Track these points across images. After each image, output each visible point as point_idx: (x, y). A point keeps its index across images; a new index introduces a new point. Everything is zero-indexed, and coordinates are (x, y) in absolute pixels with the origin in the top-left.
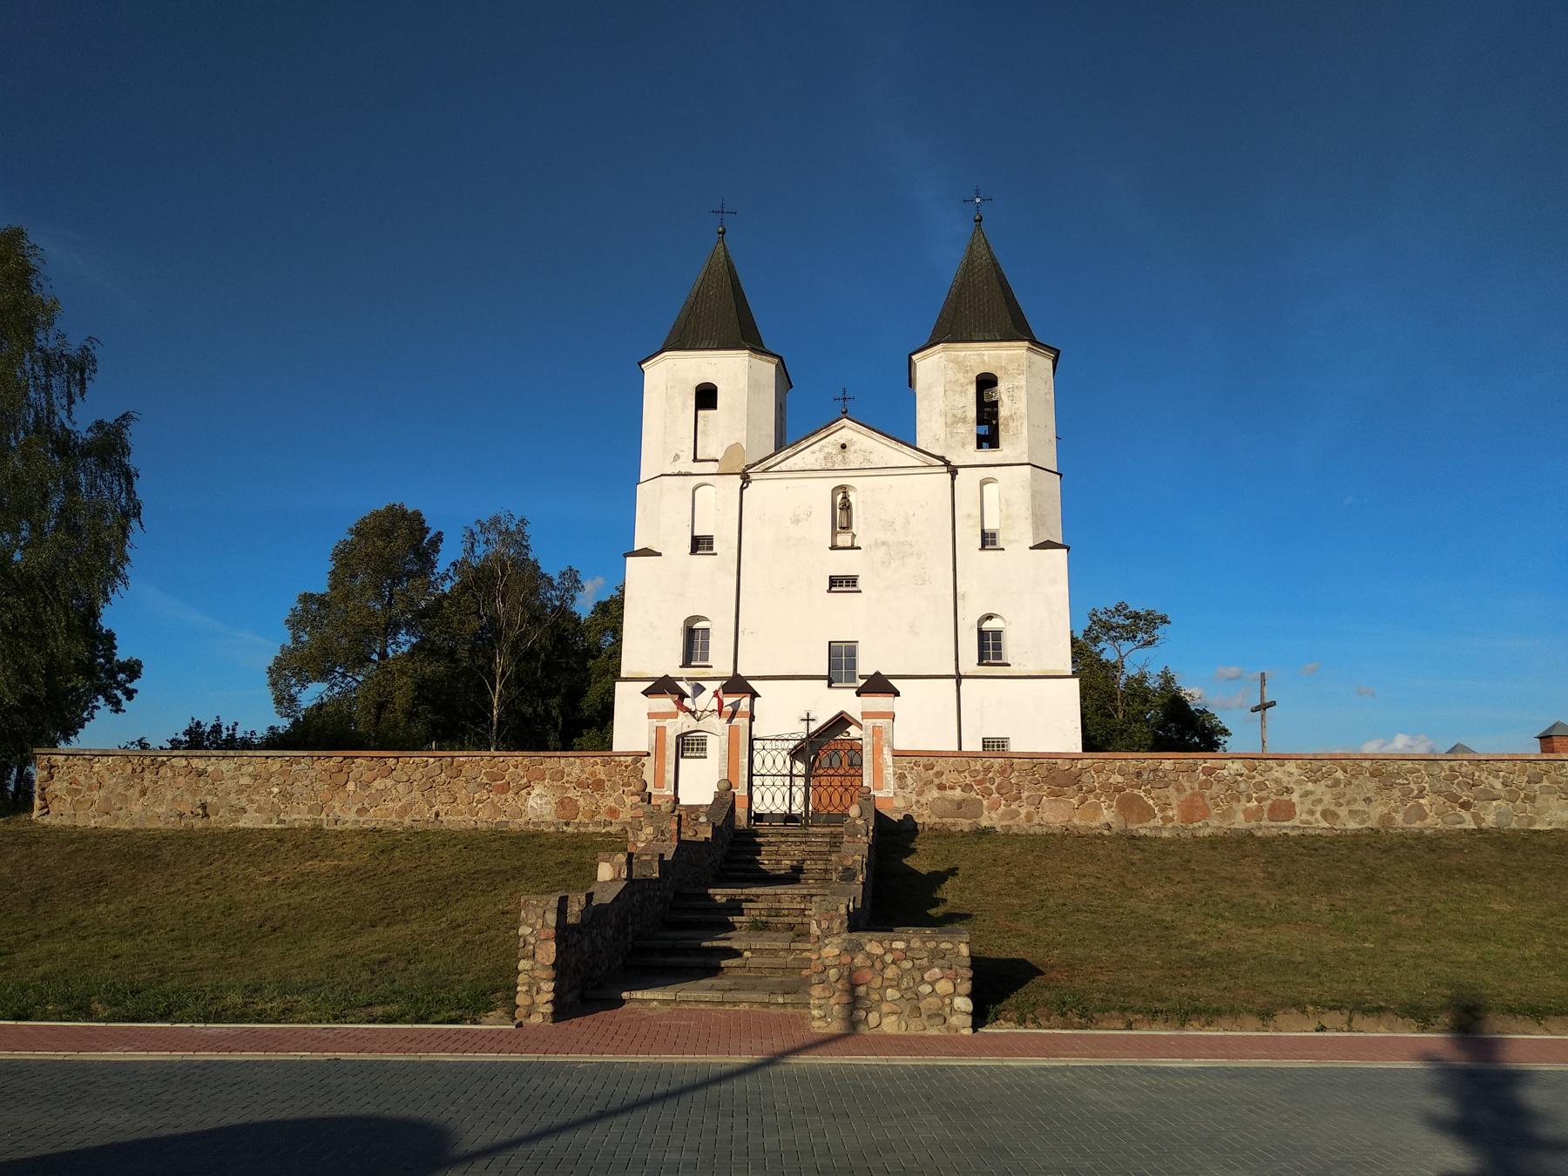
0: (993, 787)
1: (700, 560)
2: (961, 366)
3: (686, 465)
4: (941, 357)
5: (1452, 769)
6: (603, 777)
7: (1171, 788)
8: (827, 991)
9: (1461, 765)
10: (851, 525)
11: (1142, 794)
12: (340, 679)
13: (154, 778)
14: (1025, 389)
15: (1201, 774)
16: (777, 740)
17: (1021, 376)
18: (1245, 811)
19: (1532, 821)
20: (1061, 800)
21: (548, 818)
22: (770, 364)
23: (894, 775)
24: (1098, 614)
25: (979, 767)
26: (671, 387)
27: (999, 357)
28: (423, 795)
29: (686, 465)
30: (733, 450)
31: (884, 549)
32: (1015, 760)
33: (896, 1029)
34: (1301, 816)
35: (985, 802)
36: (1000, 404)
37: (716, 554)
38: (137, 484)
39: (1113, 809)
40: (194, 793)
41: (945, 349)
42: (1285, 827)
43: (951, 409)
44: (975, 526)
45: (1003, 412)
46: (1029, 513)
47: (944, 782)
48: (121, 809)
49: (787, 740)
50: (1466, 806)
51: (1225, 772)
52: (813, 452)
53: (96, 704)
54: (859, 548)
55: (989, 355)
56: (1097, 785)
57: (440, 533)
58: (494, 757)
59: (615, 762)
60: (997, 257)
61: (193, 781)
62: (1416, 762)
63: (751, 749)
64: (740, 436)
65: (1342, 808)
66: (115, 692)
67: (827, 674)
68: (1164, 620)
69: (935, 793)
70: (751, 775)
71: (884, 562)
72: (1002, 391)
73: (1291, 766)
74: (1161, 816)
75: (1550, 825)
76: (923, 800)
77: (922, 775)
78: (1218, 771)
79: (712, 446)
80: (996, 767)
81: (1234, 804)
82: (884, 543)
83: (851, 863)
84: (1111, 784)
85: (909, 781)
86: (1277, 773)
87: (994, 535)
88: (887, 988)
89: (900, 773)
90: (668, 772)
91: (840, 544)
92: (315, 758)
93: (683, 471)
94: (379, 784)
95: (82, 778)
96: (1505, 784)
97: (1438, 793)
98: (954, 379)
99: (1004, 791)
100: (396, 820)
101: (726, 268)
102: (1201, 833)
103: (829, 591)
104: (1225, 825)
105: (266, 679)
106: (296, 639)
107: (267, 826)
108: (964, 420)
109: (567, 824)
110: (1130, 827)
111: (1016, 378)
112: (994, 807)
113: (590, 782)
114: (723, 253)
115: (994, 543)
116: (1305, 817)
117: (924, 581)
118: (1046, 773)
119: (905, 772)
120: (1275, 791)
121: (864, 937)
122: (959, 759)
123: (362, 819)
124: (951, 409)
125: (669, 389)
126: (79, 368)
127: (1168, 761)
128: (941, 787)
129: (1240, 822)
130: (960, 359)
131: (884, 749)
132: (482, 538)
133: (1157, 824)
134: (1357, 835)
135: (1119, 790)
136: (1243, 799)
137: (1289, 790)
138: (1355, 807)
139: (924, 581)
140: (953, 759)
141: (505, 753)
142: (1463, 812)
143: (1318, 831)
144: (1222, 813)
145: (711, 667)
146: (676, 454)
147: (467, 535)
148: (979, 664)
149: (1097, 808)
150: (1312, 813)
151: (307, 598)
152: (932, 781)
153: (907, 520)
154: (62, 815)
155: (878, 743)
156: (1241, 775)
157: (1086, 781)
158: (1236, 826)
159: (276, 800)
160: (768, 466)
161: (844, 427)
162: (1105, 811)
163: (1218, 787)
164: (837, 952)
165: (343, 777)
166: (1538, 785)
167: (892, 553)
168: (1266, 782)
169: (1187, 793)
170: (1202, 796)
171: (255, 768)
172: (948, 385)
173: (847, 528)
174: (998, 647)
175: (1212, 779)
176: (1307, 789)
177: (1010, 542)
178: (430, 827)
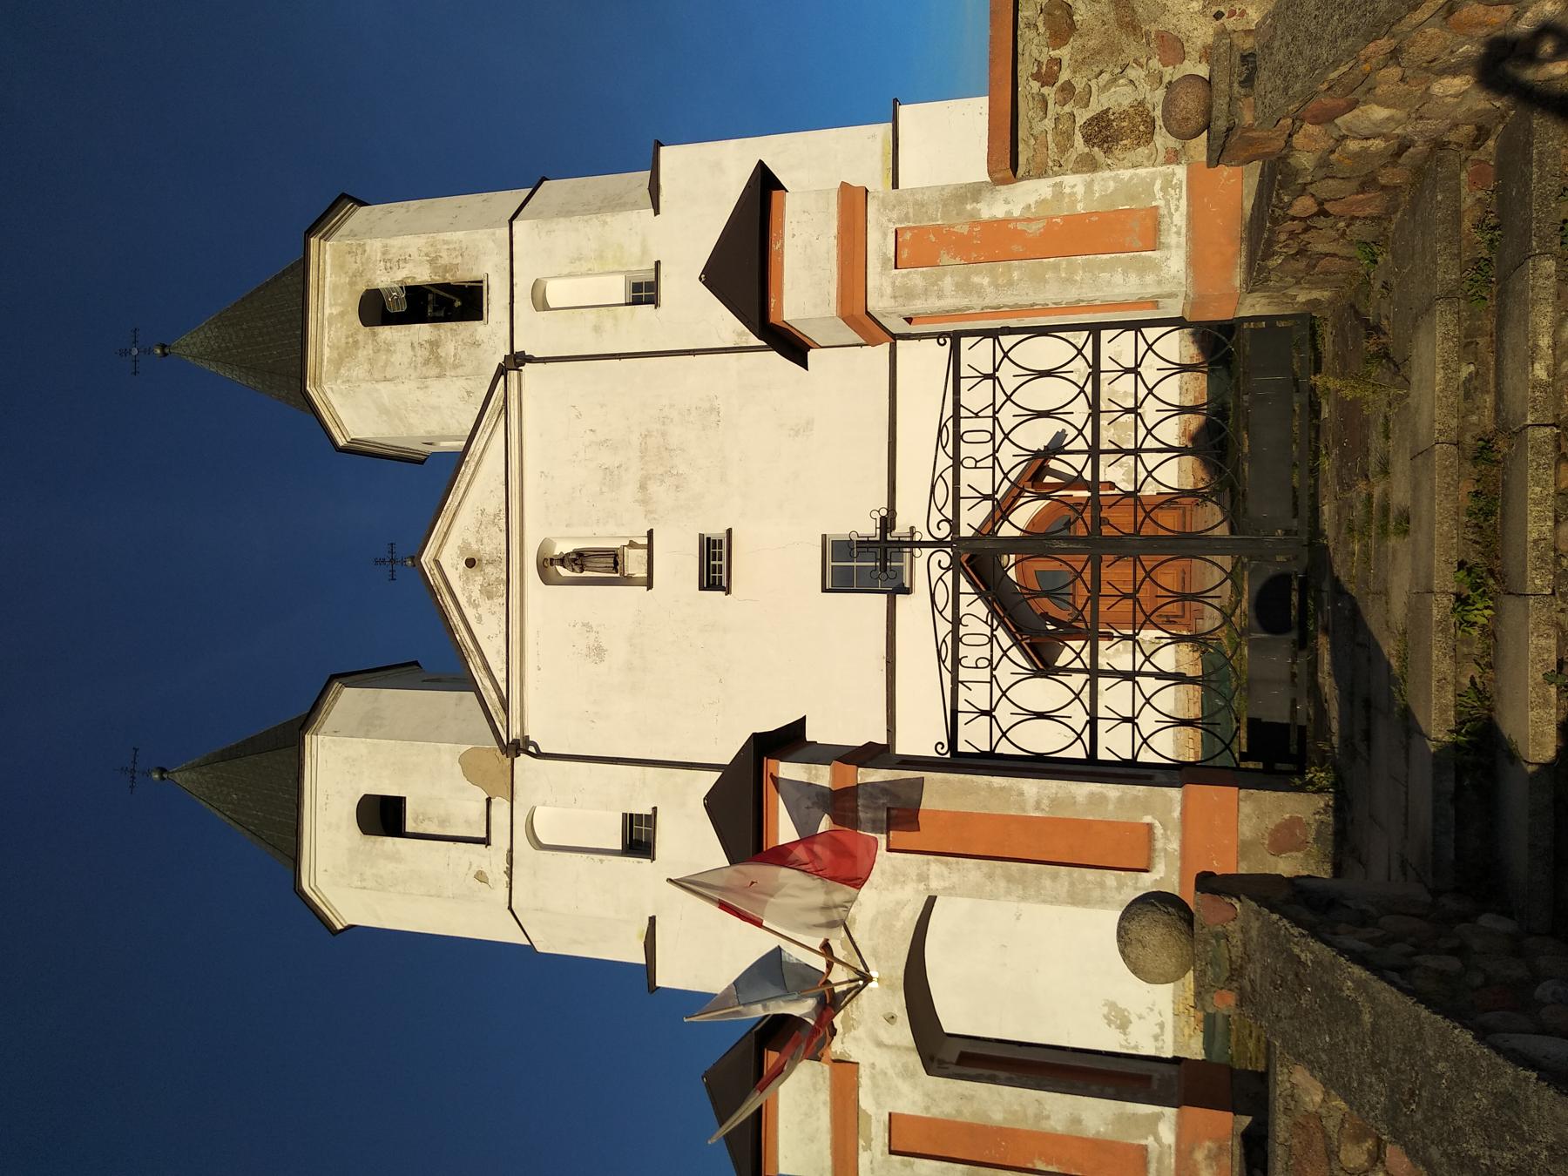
2: (346, 354)
10: (613, 550)
16: (956, 661)
17: (367, 248)
27: (335, 288)
29: (491, 859)
30: (471, 769)
31: (653, 487)
36: (410, 283)
44: (615, 318)
45: (423, 275)
46: (595, 221)
49: (956, 621)
52: (479, 619)
54: (650, 534)
55: (331, 305)
63: (989, 763)
64: (447, 755)
67: (884, 596)
70: (1091, 768)
77: (1093, 43)
79: (465, 809)
82: (643, 487)
87: (637, 287)
89: (1088, 140)
90: (1077, 1121)
98: (366, 366)
103: (728, 591)
108: (434, 344)
111: (369, 258)
117: (712, 409)
119: (1080, 121)
125: (364, 884)
139: (712, 409)
161: (437, 562)
167: (661, 470)
173: (614, 558)
177: (645, 251)
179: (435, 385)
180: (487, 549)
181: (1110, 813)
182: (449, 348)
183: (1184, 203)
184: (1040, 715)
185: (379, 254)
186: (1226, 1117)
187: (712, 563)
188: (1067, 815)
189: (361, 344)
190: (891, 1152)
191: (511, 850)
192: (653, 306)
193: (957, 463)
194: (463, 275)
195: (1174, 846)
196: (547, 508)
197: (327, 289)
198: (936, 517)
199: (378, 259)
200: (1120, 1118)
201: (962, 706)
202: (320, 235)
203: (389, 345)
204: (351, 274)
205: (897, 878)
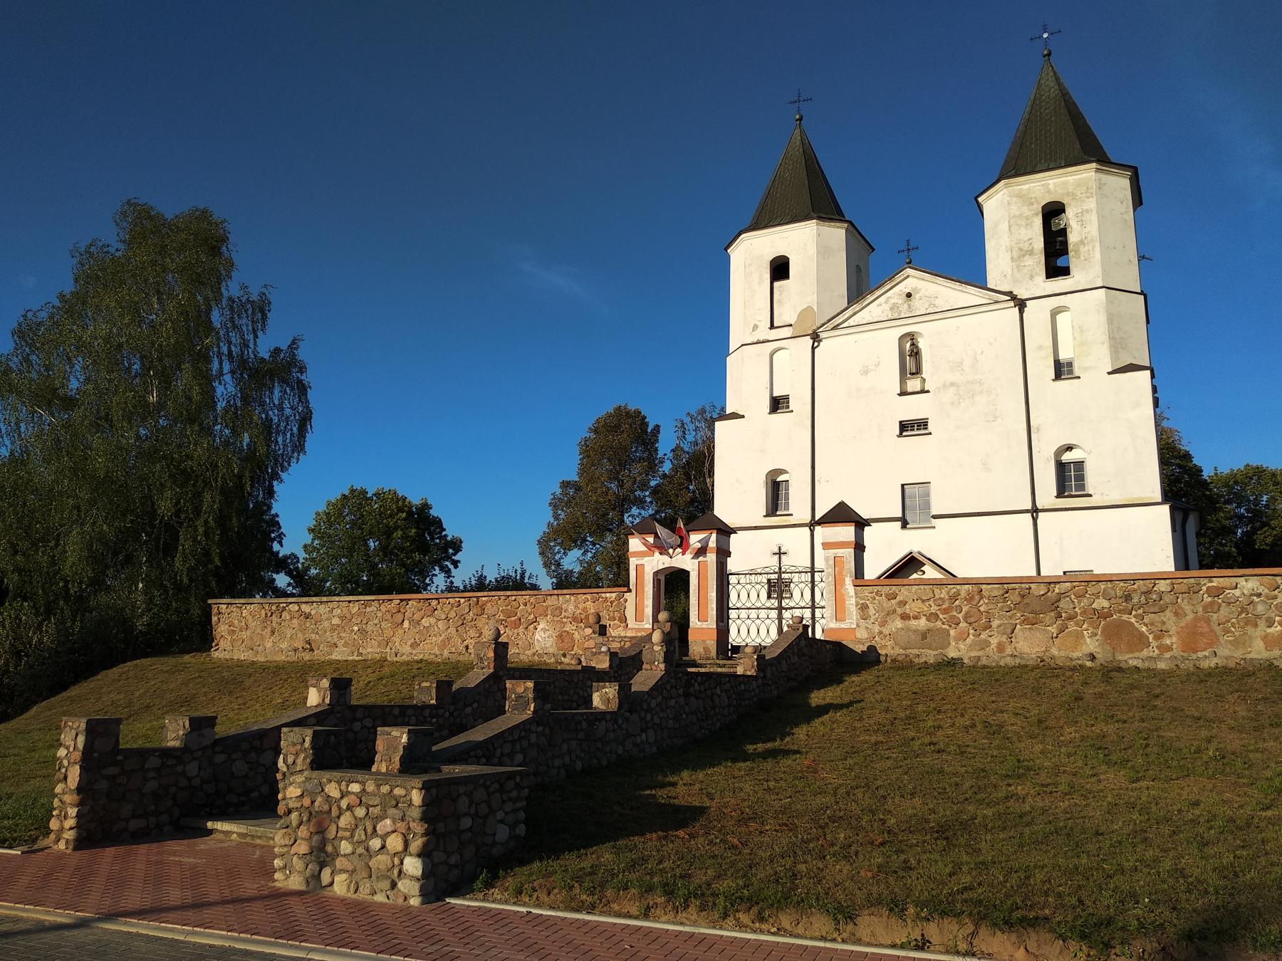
0: (960, 616)
1: (778, 417)
2: (1024, 199)
3: (765, 334)
4: (1004, 194)
7: (1168, 612)
8: (287, 838)
11: (1133, 620)
12: (591, 547)
13: (279, 620)
14: (1095, 212)
15: (1206, 596)
16: (751, 574)
18: (1265, 638)
20: (1036, 628)
21: (551, 650)
22: (840, 230)
23: (856, 606)
25: (944, 595)
26: (749, 265)
27: (1065, 183)
28: (457, 631)
30: (805, 313)
31: (952, 390)
32: (984, 587)
33: (345, 891)
35: (952, 632)
36: (1069, 230)
37: (792, 411)
38: (311, 395)
39: (1098, 637)
40: (304, 631)
41: (1006, 186)
43: (1017, 243)
45: (1073, 238)
46: (1105, 337)
47: (908, 611)
48: (259, 645)
49: (761, 574)
51: (1237, 592)
53: (434, 572)
54: (928, 392)
56: (1079, 611)
57: (658, 426)
58: (508, 596)
59: (602, 598)
60: (1066, 86)
61: (302, 623)
64: (811, 300)
66: (447, 563)
69: (899, 624)
71: (953, 403)
72: (1071, 218)
74: (1156, 644)
76: (886, 631)
78: (1228, 591)
80: (963, 594)
81: (1250, 629)
82: (952, 384)
83: (522, 691)
84: (1094, 609)
85: (872, 611)
87: (1070, 364)
88: (342, 838)
90: (647, 607)
91: (909, 390)
92: (381, 601)
93: (761, 339)
94: (425, 622)
95: (237, 621)
99: (972, 620)
100: (438, 653)
101: (801, 150)
102: (1205, 664)
103: (900, 435)
104: (1239, 654)
105: (537, 549)
106: (556, 517)
107: (350, 658)
108: (1031, 253)
109: (564, 656)
110: (1119, 657)
111: (1083, 201)
112: (962, 637)
113: (583, 617)
114: (799, 138)
115: (1071, 372)
118: (1019, 599)
121: (325, 775)
122: (922, 587)
123: (414, 652)
126: (260, 310)
128: (905, 617)
131: (846, 579)
132: (692, 427)
133: (1151, 654)
135: (1103, 615)
140: (917, 587)
141: (515, 593)
144: (1234, 640)
145: (791, 515)
147: (679, 425)
148: (1057, 497)
149: (1079, 637)
151: (565, 485)
152: (894, 611)
153: (975, 359)
154: (225, 650)
155: (841, 573)
156: (1259, 595)
157: (1066, 607)
158: (1253, 656)
159: (356, 637)
161: (908, 276)
162: (1088, 640)
163: (1227, 610)
164: (299, 792)
165: (399, 617)
167: (961, 393)
169: (1188, 617)
170: (1208, 621)
171: (342, 610)
172: (1012, 220)
173: (917, 372)
174: (1081, 478)
175: (1220, 601)
177: (1086, 369)
178: (461, 658)
179: (1008, 256)
180: (916, 303)
181: (710, 612)
182: (1029, 261)
183: (846, 627)
184: (739, 596)
185: (1086, 208)
187: (916, 425)
188: (709, 603)
189: (1031, 207)
191: (768, 341)
192: (1054, 378)
193: (800, 572)
194: (1074, 262)
195: (704, 626)
197: (1065, 178)
198: (787, 567)
199: (1083, 208)
201: (740, 576)
202: (1099, 167)
203: (1031, 224)
204: (1074, 191)
205: (693, 564)
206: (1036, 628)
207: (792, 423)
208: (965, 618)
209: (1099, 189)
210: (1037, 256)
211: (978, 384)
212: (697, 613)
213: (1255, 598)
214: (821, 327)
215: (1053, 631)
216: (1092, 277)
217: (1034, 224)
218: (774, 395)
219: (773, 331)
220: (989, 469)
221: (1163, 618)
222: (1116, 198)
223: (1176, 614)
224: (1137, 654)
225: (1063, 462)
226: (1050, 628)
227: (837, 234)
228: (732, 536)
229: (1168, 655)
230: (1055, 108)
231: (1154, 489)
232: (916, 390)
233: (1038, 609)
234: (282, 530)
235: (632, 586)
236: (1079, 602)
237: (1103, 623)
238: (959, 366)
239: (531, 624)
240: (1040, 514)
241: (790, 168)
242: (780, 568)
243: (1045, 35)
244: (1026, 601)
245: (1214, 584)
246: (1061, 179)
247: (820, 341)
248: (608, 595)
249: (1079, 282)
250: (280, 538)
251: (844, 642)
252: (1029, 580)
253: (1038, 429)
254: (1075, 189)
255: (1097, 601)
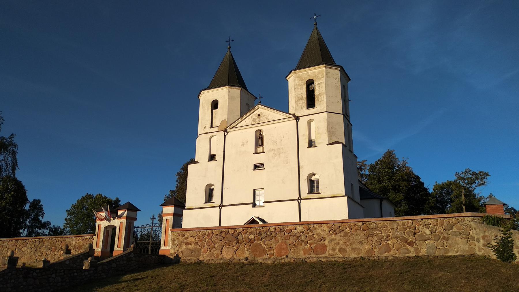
0: (205, 243)
2: (299, 78)
3: (208, 130)
5: (403, 225)
6: (81, 244)
9: (408, 222)
11: (262, 243)
14: (324, 83)
19: (447, 251)
24: (459, 174)
27: (314, 72)
28: (34, 253)
30: (223, 122)
31: (273, 152)
34: (329, 252)
37: (216, 160)
41: (294, 73)
42: (321, 257)
43: (297, 95)
45: (316, 93)
47: (188, 241)
50: (411, 244)
52: (249, 119)
55: (311, 72)
62: (385, 222)
65: (349, 247)
68: (488, 175)
69: (185, 247)
71: (273, 157)
73: (325, 227)
75: (457, 253)
78: (293, 231)
82: (273, 150)
85: (176, 242)
86: (319, 230)
91: (258, 152)
92: (9, 241)
93: (207, 132)
96: (432, 232)
97: (397, 238)
99: (209, 244)
101: (228, 59)
108: (302, 99)
110: (256, 259)
111: (321, 79)
113: (78, 246)
114: (228, 55)
116: (330, 252)
120: (317, 239)
124: (297, 95)
127: (272, 227)
128: (187, 244)
129: (301, 255)
130: (300, 76)
134: (354, 260)
136: (303, 244)
137: (323, 239)
138: (355, 246)
139: (287, 162)
140: (191, 231)
141: (55, 236)
142: (410, 248)
143: (336, 259)
145: (214, 202)
146: (205, 126)
148: (308, 194)
149: (243, 250)
150: (334, 250)
152: (183, 242)
153: (281, 139)
158: (300, 257)
160: (233, 126)
161: (259, 108)
162: (246, 252)
166: (450, 231)
167: (276, 153)
168: (314, 235)
172: (296, 86)
173: (262, 145)
176: (332, 238)
177: (319, 143)
186: (100, 255)
189: (302, 82)
190: (99, 225)
191: (209, 133)
195: (119, 250)
196: (269, 130)
197: (314, 70)
200: (100, 245)
206: (230, 247)
207: (217, 165)
208: (207, 244)
209: (327, 74)
210: (304, 100)
211: (282, 149)
212: (117, 244)
213: (302, 233)
214: (228, 127)
215: (235, 248)
216: (323, 108)
217: (303, 88)
218: (211, 154)
219: (211, 129)
220: (284, 183)
221: (271, 242)
222: (333, 78)
223: (276, 240)
224: (261, 258)
225: (312, 180)
226: (234, 247)
227: (237, 92)
228: (138, 212)
229: (272, 258)
230: (315, 44)
231: (343, 192)
232: (261, 152)
233: (231, 239)
234: (44, 211)
235: (96, 233)
236: (245, 236)
237: (252, 245)
238: (276, 142)
239: (60, 250)
240: (302, 200)
241: (223, 66)
242: (153, 224)
243: (315, 17)
244: (227, 236)
245: (288, 228)
246: (321, 69)
247: (227, 133)
248: (87, 237)
249: (318, 110)
250: (43, 214)
251: (166, 255)
252: (215, 228)
253: (302, 167)
254: (318, 74)
255: (250, 236)
